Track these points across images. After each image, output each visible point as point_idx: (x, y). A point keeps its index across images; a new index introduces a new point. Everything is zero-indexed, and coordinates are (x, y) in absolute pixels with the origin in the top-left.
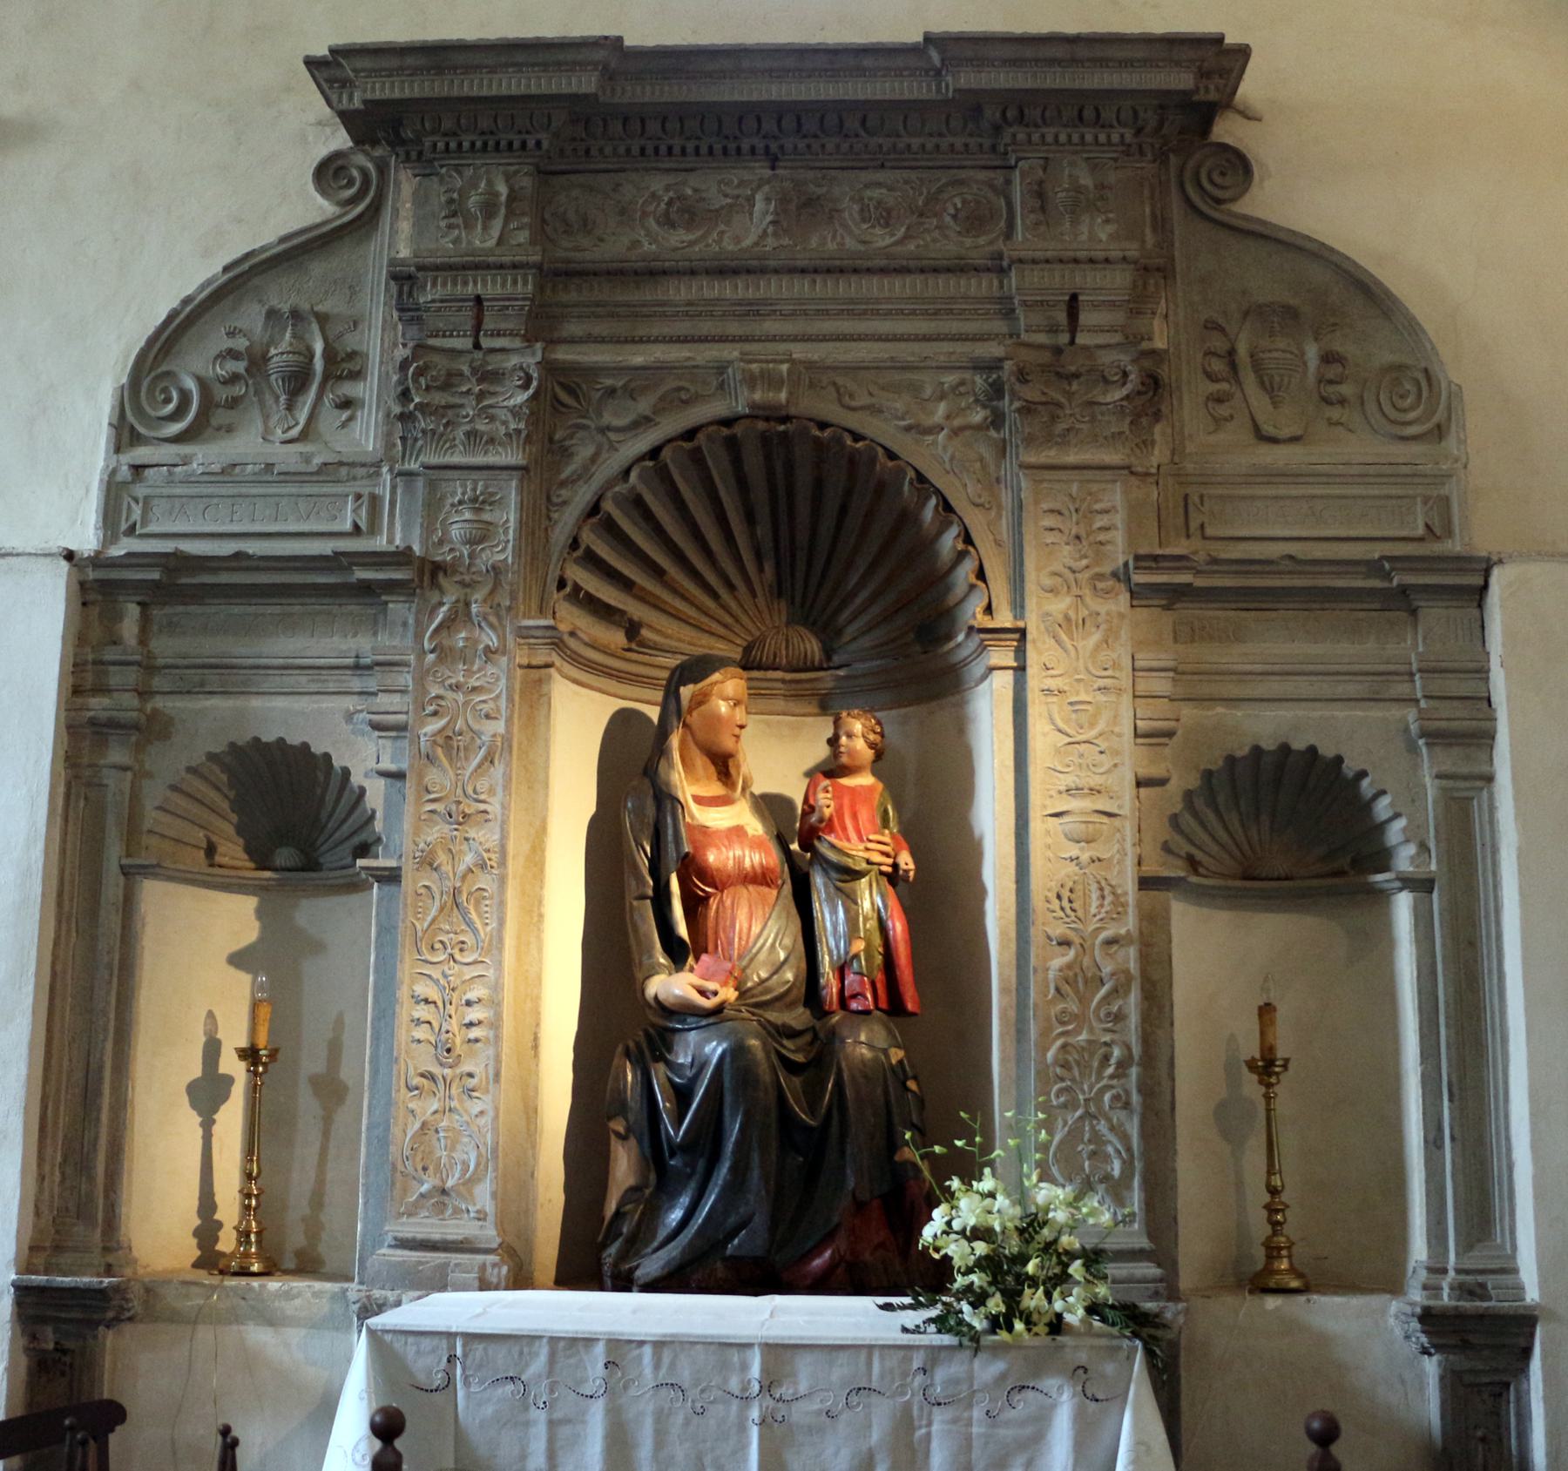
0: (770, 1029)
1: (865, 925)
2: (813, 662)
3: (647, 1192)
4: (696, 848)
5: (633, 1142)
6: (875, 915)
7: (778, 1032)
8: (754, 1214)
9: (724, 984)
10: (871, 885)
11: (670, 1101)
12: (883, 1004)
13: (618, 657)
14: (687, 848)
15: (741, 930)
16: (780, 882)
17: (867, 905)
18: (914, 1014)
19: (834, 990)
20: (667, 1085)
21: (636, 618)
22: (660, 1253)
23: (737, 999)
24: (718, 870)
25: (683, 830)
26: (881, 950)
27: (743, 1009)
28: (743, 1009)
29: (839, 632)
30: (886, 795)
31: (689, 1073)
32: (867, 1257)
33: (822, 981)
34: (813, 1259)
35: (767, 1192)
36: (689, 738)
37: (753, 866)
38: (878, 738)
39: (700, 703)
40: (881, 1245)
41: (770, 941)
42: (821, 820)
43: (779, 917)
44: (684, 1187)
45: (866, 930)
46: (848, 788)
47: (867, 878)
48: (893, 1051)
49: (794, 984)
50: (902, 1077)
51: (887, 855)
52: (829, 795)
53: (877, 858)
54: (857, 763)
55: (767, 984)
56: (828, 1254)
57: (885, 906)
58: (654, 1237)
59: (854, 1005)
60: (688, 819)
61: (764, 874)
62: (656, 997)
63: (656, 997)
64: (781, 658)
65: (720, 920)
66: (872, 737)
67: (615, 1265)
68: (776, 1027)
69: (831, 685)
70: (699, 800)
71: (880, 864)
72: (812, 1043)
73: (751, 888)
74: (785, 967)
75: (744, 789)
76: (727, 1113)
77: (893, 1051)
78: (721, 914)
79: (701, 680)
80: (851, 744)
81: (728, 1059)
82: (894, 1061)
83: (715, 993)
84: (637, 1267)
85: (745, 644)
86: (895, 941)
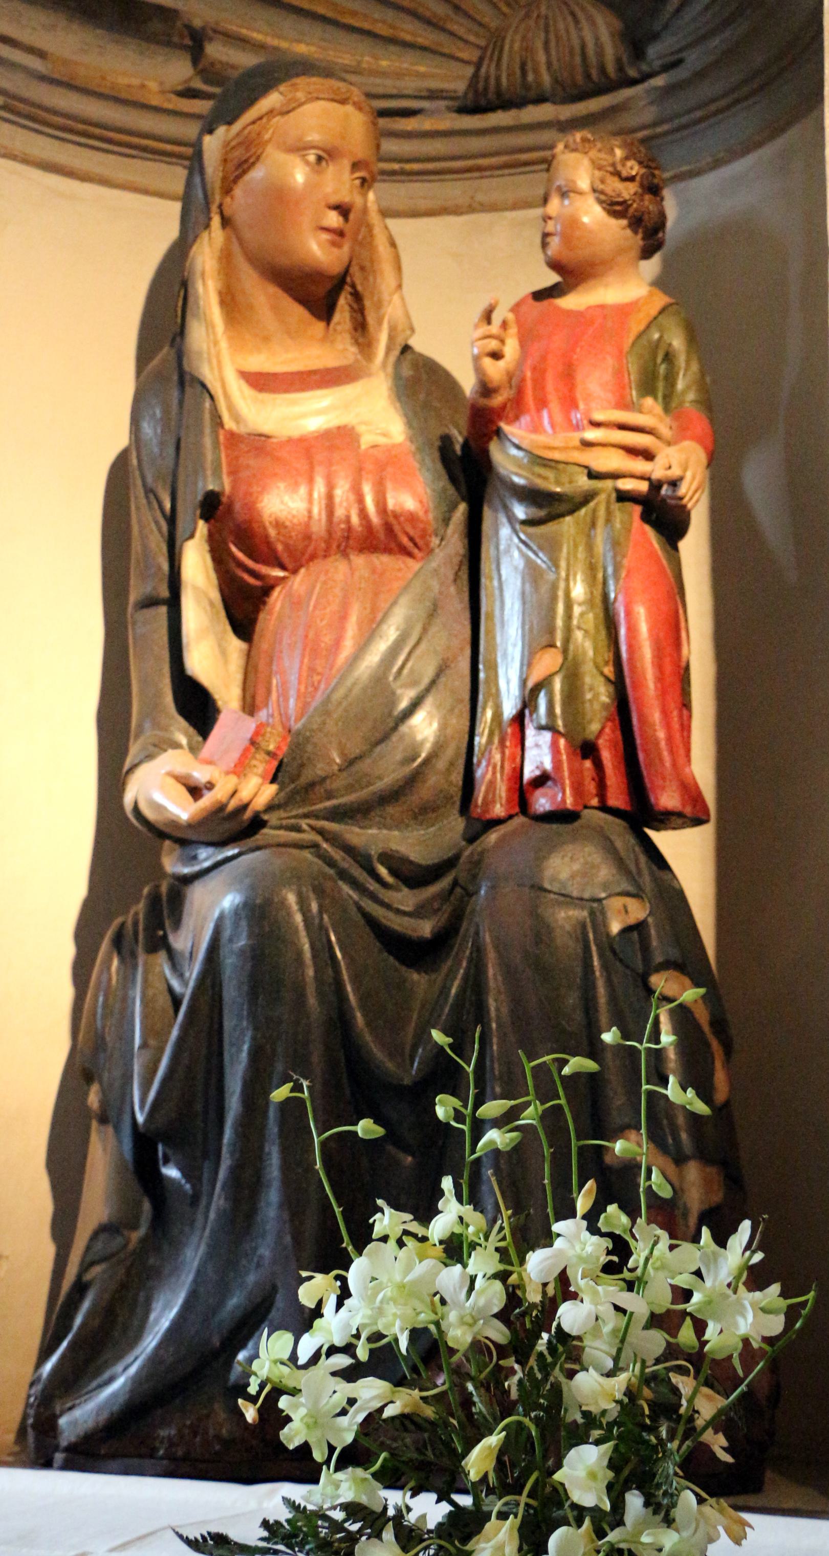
2: (603, 70)
3: (136, 1236)
8: (274, 1289)
12: (617, 800)
13: (157, 110)
21: (197, 23)
28: (304, 825)
39: (244, 166)
46: (569, 313)
50: (640, 967)
59: (542, 802)
61: (389, 529)
62: (136, 810)
64: (536, 71)
69: (649, 114)
82: (615, 927)
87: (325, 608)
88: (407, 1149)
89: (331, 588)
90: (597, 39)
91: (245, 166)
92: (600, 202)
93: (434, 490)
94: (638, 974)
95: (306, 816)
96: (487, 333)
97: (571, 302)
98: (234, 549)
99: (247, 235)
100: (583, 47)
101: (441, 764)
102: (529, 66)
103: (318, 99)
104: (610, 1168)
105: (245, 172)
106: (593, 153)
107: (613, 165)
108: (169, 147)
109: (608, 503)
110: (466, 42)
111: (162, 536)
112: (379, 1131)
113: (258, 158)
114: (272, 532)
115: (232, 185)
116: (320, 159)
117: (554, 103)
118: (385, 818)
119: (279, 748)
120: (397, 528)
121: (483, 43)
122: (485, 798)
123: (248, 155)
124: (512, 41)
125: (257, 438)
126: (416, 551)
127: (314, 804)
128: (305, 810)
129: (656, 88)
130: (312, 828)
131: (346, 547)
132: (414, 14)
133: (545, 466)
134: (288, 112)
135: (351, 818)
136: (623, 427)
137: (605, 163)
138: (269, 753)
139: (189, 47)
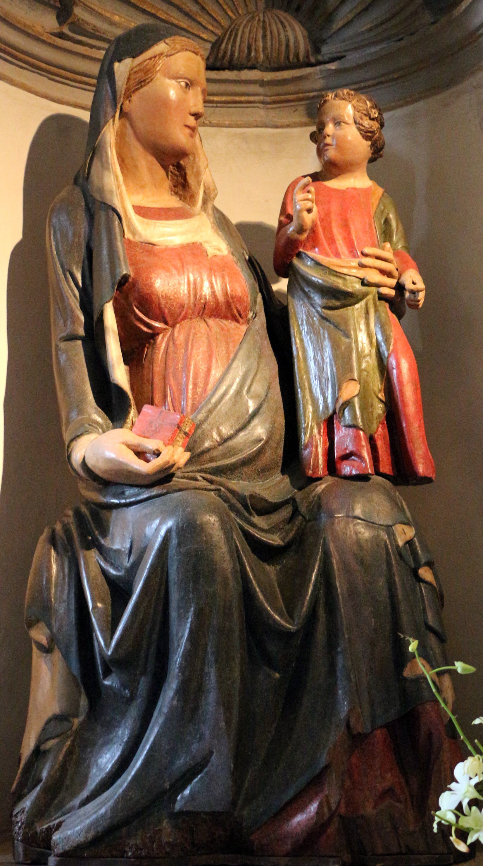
0: (234, 501)
1: (359, 363)
2: (297, 55)
3: (76, 722)
4: (137, 272)
5: (57, 655)
6: (374, 351)
7: (246, 506)
8: (211, 753)
9: (171, 442)
10: (367, 313)
11: (102, 601)
12: (386, 467)
13: (43, 42)
14: (125, 269)
15: (196, 374)
16: (250, 315)
17: (362, 337)
18: (427, 480)
19: (320, 450)
20: (101, 579)
22: (89, 807)
23: (189, 462)
24: (166, 297)
25: (119, 245)
26: (381, 396)
27: (198, 476)
28: (198, 476)
29: (329, 18)
30: (388, 201)
31: (127, 563)
32: (369, 810)
33: (304, 438)
34: (294, 815)
35: (228, 723)
36: (130, 131)
37: (213, 293)
38: (375, 125)
39: (142, 83)
40: (389, 792)
41: (234, 387)
42: (301, 230)
43: (248, 357)
44: (123, 715)
45: (360, 371)
47: (363, 303)
48: (399, 528)
49: (267, 442)
51: (389, 275)
52: (310, 196)
53: (375, 277)
54: (349, 157)
55: (230, 443)
56: (313, 807)
57: (387, 340)
58: (83, 784)
59: (347, 469)
60: (128, 235)
61: (228, 304)
62: (84, 463)
63: (84, 463)
64: (256, 51)
65: (170, 363)
66: (367, 123)
67: (30, 824)
68: (242, 499)
70: (140, 211)
71: (378, 286)
72: (291, 520)
73: (211, 321)
74: (256, 421)
75: (205, 202)
76: (173, 614)
77: (399, 528)
78: (171, 355)
79: (141, 53)
80: (340, 132)
81: (174, 541)
82: (401, 543)
83: (157, 454)
84: (58, 826)
85: (213, 39)
86: (400, 382)
87: (199, 349)
88: (275, 669)
89: (200, 337)
90: (296, 37)
91: (143, 84)
92: (359, 129)
93: (250, 285)
94: (411, 568)
95: (199, 471)
96: (306, 197)
97: (333, 184)
98: (137, 311)
99: (139, 124)
100: (288, 41)
101: (273, 444)
102: (253, 47)
103: (187, 50)
104: (405, 679)
105: (142, 87)
106: (354, 102)
107: (367, 110)
108: (44, 65)
109: (374, 300)
110: (206, 28)
111: (76, 298)
112: (471, 669)
113: (152, 80)
114: (163, 302)
115: (131, 94)
116: (187, 85)
117: (261, 71)
118: (242, 475)
119: (190, 431)
120: (233, 306)
121: (219, 32)
122: (313, 466)
123: (147, 77)
124: (243, 32)
125: (147, 245)
126: (240, 319)
127: (203, 465)
128: (199, 468)
129: (330, 70)
130: (204, 478)
131: (203, 313)
132: (179, 9)
133: (337, 276)
134: (170, 56)
135: (225, 474)
136: (378, 258)
137: (361, 108)
138: (185, 433)
139: (57, 8)
